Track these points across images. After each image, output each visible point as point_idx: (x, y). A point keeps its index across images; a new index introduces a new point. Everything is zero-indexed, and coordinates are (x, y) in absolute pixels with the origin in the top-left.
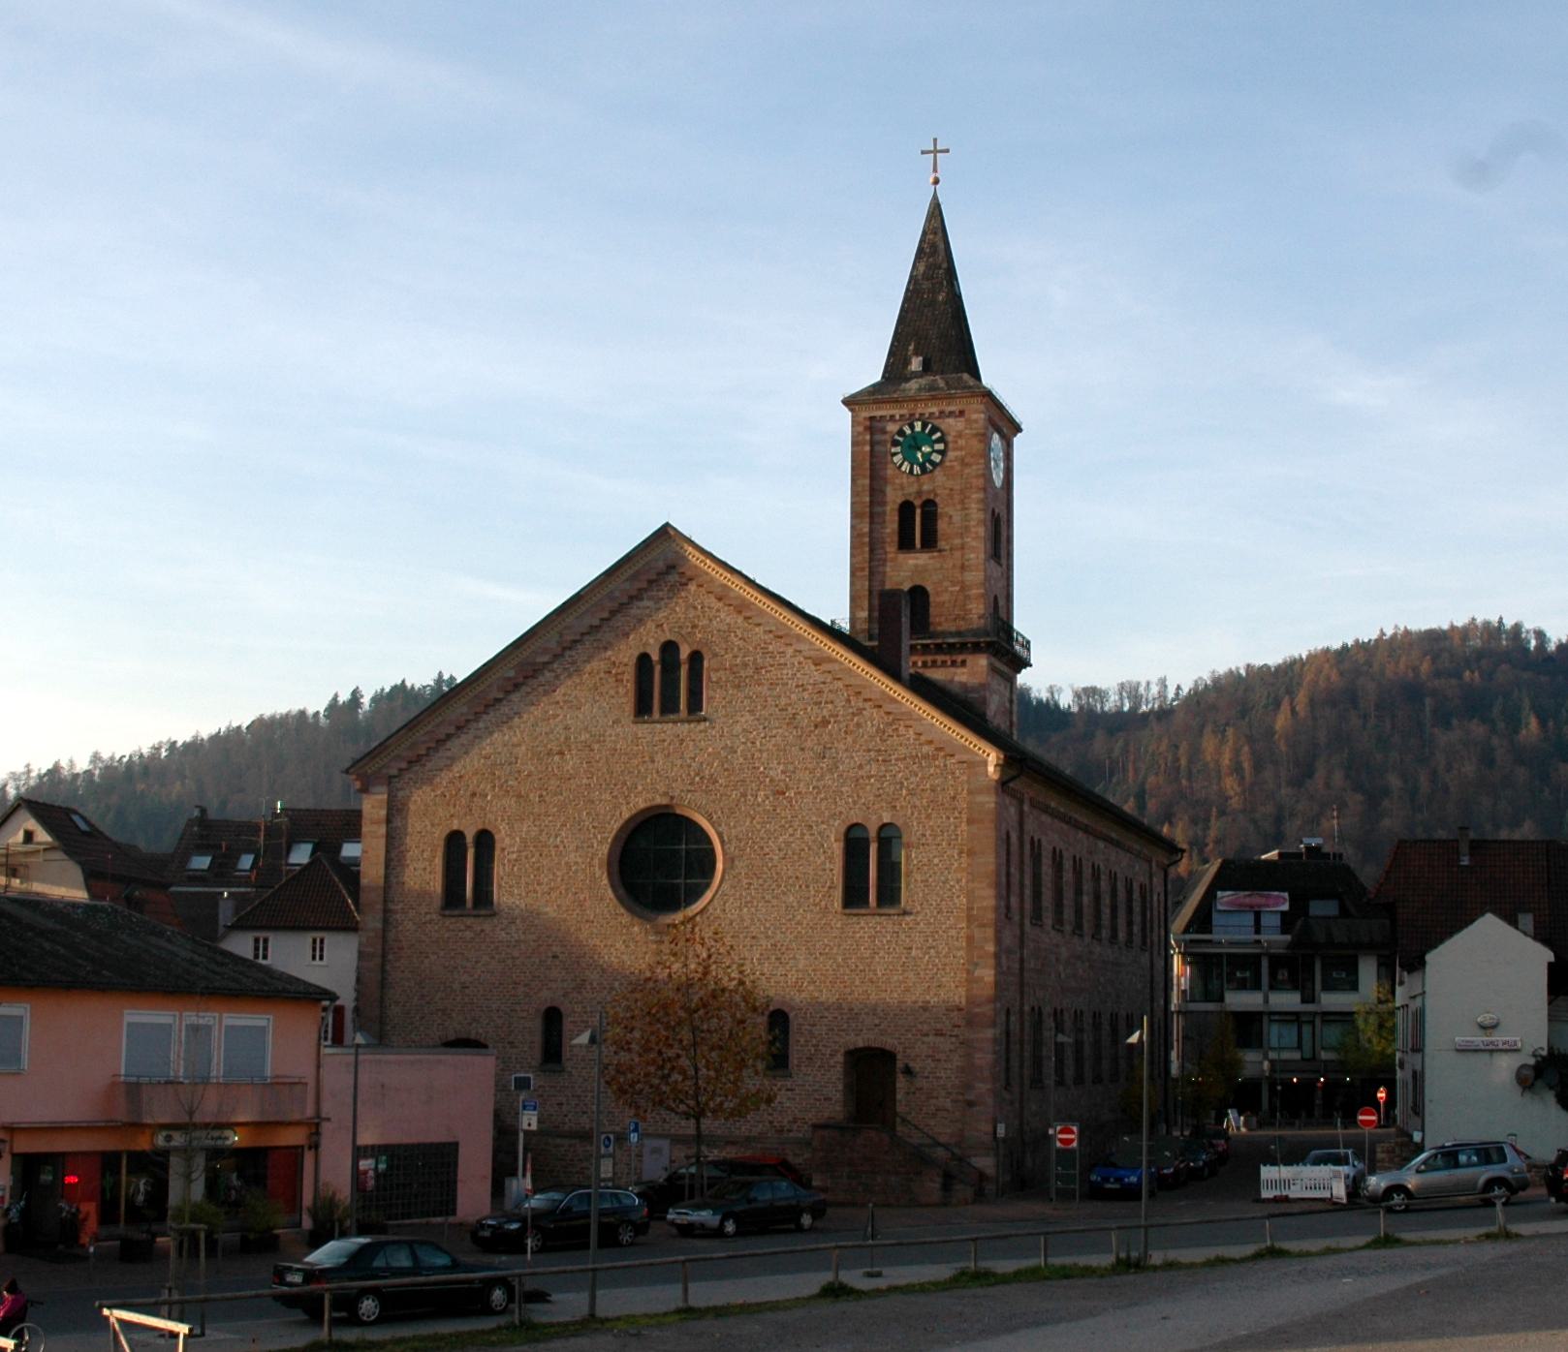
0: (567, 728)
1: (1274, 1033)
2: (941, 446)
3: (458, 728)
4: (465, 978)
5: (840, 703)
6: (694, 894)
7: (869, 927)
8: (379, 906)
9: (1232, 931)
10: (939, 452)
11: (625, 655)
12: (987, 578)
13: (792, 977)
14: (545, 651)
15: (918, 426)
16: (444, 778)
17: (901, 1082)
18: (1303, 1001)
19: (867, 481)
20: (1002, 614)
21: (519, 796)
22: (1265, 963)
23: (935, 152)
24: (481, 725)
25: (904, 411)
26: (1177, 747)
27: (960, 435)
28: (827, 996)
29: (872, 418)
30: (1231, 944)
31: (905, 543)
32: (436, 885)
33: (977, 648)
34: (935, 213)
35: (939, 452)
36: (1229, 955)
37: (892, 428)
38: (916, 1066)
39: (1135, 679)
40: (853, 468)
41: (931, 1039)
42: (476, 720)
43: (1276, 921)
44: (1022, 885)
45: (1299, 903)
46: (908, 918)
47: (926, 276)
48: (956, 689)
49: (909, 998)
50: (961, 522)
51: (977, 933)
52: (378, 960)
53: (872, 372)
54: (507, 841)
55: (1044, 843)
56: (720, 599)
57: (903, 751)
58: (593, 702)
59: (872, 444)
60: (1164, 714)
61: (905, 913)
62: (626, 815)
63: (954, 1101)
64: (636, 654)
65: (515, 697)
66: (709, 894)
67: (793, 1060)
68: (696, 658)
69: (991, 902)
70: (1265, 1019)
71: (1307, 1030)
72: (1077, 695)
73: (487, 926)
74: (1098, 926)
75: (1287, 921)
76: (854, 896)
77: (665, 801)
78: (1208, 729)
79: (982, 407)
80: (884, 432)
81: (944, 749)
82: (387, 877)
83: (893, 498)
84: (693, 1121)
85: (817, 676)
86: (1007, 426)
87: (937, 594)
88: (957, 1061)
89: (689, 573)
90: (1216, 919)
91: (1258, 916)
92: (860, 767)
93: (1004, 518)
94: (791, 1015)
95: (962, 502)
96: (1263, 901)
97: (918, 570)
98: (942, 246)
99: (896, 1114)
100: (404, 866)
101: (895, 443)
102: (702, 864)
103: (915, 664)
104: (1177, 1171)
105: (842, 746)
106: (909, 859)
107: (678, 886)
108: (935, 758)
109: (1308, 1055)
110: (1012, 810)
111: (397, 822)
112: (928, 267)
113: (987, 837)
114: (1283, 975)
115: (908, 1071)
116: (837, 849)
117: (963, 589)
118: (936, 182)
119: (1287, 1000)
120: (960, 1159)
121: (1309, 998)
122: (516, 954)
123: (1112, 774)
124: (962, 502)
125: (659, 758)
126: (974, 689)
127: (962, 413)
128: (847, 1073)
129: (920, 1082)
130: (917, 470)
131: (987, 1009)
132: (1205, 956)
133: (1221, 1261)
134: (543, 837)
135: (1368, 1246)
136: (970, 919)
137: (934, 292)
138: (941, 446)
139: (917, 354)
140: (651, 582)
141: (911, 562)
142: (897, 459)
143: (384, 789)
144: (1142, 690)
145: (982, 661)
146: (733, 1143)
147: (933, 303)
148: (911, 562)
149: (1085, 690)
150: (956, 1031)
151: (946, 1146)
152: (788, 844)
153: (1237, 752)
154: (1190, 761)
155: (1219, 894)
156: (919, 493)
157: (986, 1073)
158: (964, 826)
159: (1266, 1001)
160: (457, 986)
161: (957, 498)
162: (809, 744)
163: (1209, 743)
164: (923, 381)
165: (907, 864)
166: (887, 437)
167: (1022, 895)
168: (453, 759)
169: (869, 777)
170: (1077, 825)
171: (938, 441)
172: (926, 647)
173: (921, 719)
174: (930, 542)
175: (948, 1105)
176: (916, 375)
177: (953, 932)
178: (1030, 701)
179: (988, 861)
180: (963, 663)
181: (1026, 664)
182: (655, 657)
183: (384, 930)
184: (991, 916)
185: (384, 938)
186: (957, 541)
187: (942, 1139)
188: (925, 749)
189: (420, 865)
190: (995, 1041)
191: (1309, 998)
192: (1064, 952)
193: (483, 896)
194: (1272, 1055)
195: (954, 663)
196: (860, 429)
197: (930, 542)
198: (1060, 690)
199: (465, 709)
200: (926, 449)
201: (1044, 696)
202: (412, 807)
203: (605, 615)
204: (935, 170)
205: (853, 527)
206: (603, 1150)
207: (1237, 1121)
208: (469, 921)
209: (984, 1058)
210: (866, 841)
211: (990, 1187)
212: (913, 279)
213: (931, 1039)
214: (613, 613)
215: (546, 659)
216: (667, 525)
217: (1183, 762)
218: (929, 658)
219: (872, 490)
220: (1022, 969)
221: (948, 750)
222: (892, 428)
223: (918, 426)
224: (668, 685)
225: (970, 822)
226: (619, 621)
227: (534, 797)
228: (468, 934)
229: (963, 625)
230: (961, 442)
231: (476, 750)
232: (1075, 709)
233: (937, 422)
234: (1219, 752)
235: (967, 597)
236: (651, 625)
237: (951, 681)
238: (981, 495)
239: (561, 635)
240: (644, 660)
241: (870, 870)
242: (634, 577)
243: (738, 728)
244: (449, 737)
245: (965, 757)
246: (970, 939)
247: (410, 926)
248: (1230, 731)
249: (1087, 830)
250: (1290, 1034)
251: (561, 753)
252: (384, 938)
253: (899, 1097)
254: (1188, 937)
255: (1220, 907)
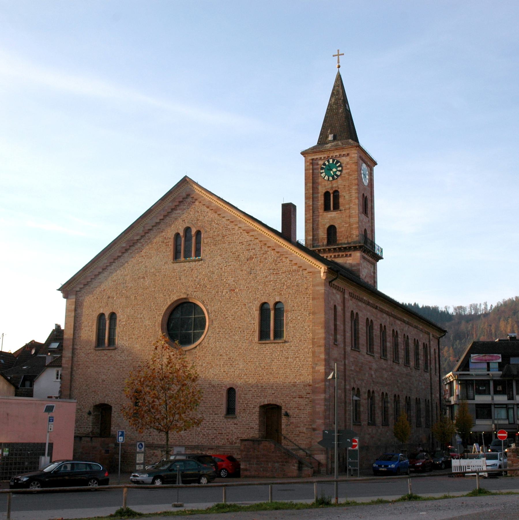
0: (146, 267)
1: (495, 412)
2: (340, 169)
3: (103, 269)
4: (104, 377)
5: (257, 249)
6: (197, 336)
7: (271, 349)
8: (71, 347)
9: (478, 369)
10: (339, 171)
11: (170, 233)
12: (359, 221)
13: (237, 373)
14: (138, 234)
15: (331, 161)
16: (98, 291)
17: (284, 420)
18: (509, 399)
19: (311, 185)
20: (369, 236)
21: (127, 297)
22: (492, 384)
23: (339, 55)
24: (113, 267)
25: (326, 156)
26: (491, 326)
27: (348, 163)
28: (251, 381)
29: (313, 159)
30: (477, 375)
31: (327, 208)
32: (93, 337)
33: (355, 249)
34: (339, 78)
35: (339, 171)
36: (476, 380)
37: (321, 162)
38: (290, 412)
39: (475, 303)
40: (305, 179)
41: (297, 399)
42: (110, 266)
43: (497, 366)
44: (344, 331)
45: (506, 359)
46: (287, 344)
47: (336, 103)
48: (347, 266)
49: (287, 381)
50: (350, 200)
51: (317, 349)
52: (70, 370)
53: (313, 141)
54: (122, 317)
55: (360, 315)
56: (208, 207)
57: (284, 268)
58: (156, 255)
59: (313, 169)
60: (486, 315)
61: (285, 342)
62: (169, 303)
63: (307, 428)
64: (174, 233)
65: (126, 255)
66: (203, 337)
67: (237, 410)
68: (198, 233)
69: (322, 335)
70: (493, 407)
71: (511, 412)
72: (455, 309)
73: (113, 353)
74: (384, 350)
75: (501, 366)
76: (263, 335)
77: (185, 296)
78: (502, 319)
79: (356, 152)
80: (318, 164)
81: (302, 267)
82: (74, 334)
83: (322, 190)
84: (163, 434)
85: (248, 238)
86: (371, 163)
87: (340, 228)
88: (308, 409)
89: (195, 197)
90: (471, 366)
91: (488, 364)
92: (266, 277)
93: (369, 197)
94: (236, 390)
95: (349, 190)
96: (490, 358)
97: (332, 219)
98: (341, 91)
99: (282, 435)
100: (81, 329)
101: (322, 168)
102: (201, 324)
103: (331, 256)
104: (423, 464)
105: (258, 268)
106: (287, 317)
107: (190, 334)
108: (298, 271)
109: (512, 421)
110: (338, 296)
111: (79, 311)
112: (336, 100)
113: (321, 304)
114: (499, 388)
115: (287, 415)
116: (256, 314)
117: (350, 225)
118: (339, 67)
119: (502, 399)
120: (310, 456)
121: (511, 398)
122: (124, 366)
123: (468, 336)
124: (349, 190)
125: (182, 278)
126: (354, 266)
127: (348, 154)
128: (260, 416)
129: (293, 420)
130: (331, 178)
131: (321, 385)
132: (466, 380)
133: (381, 502)
134: (136, 315)
135: (467, 495)
136: (313, 343)
137: (338, 109)
138: (340, 169)
139: (331, 134)
140: (180, 202)
141: (329, 216)
142: (323, 175)
143: (74, 297)
144: (478, 307)
145: (358, 254)
146: (212, 449)
147: (337, 114)
148: (329, 216)
149: (458, 307)
150: (308, 396)
151: (303, 450)
152: (235, 313)
153: (512, 327)
154: (495, 331)
155: (472, 355)
156: (332, 188)
157: (321, 415)
158: (311, 301)
159: (493, 399)
160: (100, 381)
161: (347, 189)
162: (245, 268)
163: (502, 324)
164: (333, 144)
165: (286, 320)
166: (319, 166)
167: (344, 335)
168: (101, 283)
169: (270, 281)
170: (382, 311)
171: (339, 166)
172: (335, 249)
173: (291, 254)
174: (336, 207)
175: (305, 430)
176: (330, 142)
177: (306, 350)
178: (438, 311)
179: (321, 317)
180: (350, 255)
181: (381, 258)
182: (182, 234)
183: (72, 357)
184: (322, 342)
185: (72, 360)
186: (347, 206)
187: (303, 446)
188: (294, 267)
189: (87, 329)
190: (325, 400)
191: (511, 398)
192: (374, 366)
193: (112, 341)
194: (496, 422)
195: (346, 255)
196: (308, 164)
197: (336, 207)
198: (449, 307)
199: (106, 261)
200: (334, 170)
201: (443, 310)
202: (85, 304)
203: (162, 217)
204: (338, 62)
205: (306, 203)
206: (138, 450)
207: (479, 449)
208: (105, 352)
209: (320, 408)
210: (269, 310)
211: (323, 469)
212: (330, 105)
213: (297, 399)
214: (165, 216)
215: (138, 237)
216: (186, 177)
217: (493, 331)
218: (337, 254)
219: (313, 188)
220: (345, 369)
221: (303, 268)
222: (321, 162)
223: (331, 161)
224: (187, 246)
225: (313, 299)
226: (168, 220)
227: (132, 297)
228: (106, 358)
229: (350, 240)
230: (348, 166)
231: (110, 278)
232: (454, 314)
233: (338, 159)
234: (506, 327)
235: (351, 229)
236: (180, 221)
237: (346, 263)
238: (356, 187)
239: (144, 227)
240: (177, 235)
241: (271, 323)
242: (174, 200)
243: (215, 263)
244: (100, 273)
245: (311, 270)
246: (314, 353)
247: (83, 355)
248: (510, 320)
249: (388, 314)
250: (503, 413)
251: (144, 278)
252: (72, 360)
253: (283, 427)
254: (459, 373)
255: (472, 361)
